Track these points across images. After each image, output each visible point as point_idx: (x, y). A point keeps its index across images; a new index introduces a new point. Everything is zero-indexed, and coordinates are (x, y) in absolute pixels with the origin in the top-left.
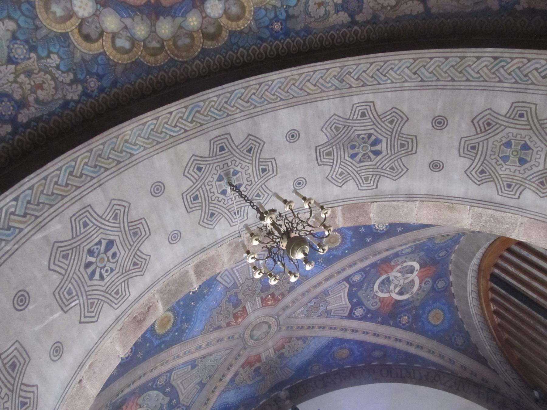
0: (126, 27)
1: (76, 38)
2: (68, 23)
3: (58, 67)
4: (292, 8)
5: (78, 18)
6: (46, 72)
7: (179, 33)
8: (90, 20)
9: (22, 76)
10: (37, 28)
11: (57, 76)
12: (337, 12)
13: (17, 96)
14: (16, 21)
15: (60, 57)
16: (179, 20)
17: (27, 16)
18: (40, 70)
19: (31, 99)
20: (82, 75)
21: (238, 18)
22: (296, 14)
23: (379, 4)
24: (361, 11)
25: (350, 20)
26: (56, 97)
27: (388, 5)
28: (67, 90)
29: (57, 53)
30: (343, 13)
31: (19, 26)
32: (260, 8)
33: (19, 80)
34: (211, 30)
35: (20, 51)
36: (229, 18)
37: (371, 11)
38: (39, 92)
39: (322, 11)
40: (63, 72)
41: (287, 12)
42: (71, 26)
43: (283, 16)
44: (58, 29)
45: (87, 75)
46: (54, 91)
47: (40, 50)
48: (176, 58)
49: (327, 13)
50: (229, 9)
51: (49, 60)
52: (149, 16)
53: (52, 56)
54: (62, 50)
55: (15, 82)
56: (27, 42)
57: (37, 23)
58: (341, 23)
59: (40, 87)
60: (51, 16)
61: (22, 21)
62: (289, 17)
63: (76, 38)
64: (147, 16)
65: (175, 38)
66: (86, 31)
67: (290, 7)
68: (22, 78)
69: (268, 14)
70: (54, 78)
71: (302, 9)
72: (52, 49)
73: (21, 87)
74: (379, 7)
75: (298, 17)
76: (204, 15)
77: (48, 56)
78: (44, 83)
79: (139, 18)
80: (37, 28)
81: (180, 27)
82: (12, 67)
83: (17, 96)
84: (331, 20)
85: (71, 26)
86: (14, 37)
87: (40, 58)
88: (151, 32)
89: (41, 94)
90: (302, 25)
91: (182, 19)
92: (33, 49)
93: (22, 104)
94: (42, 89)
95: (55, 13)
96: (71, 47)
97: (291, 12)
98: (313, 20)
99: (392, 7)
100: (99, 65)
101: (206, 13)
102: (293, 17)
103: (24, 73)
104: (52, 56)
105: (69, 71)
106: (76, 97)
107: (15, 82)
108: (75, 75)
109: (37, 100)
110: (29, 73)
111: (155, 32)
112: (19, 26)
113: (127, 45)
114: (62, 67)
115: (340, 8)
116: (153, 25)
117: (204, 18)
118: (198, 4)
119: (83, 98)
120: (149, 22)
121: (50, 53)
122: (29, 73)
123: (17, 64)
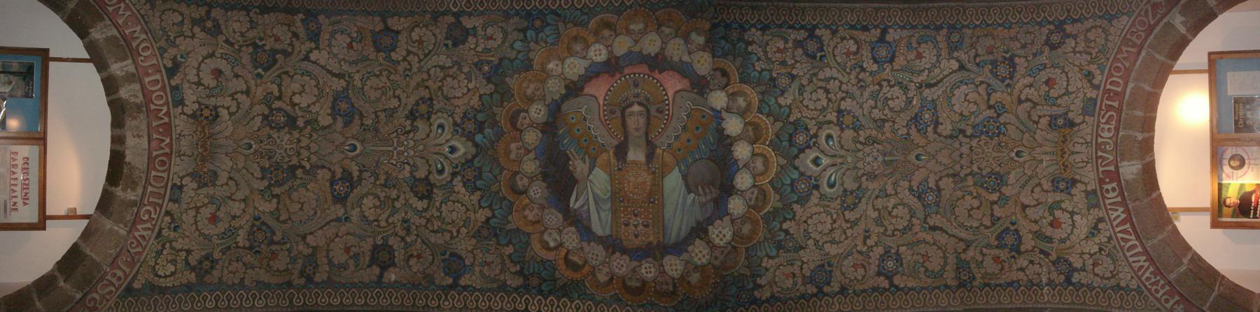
0: (690, 53)
1: (735, 76)
2: (736, 90)
3: (759, 59)
4: (520, 38)
5: (726, 91)
6: (770, 59)
7: (640, 36)
8: (717, 87)
9: (789, 63)
10: (763, 93)
11: (762, 53)
12: (474, 28)
13: (800, 51)
14: (777, 102)
15: (754, 66)
16: (637, 49)
17: (767, 103)
18: (773, 62)
19: (790, 44)
20: (740, 47)
21: (576, 39)
22: (516, 32)
23: (431, 31)
24: (449, 26)
25: (461, 19)
26: (770, 37)
27: (421, 28)
28: (758, 39)
29: (755, 70)
30: (468, 27)
31: (776, 98)
32: (552, 44)
33: (793, 62)
34: (606, 33)
35: (784, 81)
36: (585, 41)
37: (439, 24)
38: (782, 47)
39: (490, 31)
40: (756, 54)
41: (525, 36)
42: (735, 86)
43: (530, 33)
44: (747, 88)
45: (736, 45)
46: (769, 43)
47: (768, 77)
48: (648, 270)
49: (485, 28)
50: (583, 49)
51: (764, 67)
52: (665, 58)
53: (760, 70)
54: (750, 71)
55: (796, 62)
56: (775, 86)
57: (760, 97)
58: (472, 17)
59: (779, 51)
60: (748, 99)
61: (772, 102)
62: (524, 31)
63: (735, 76)
64: (666, 59)
65: (644, 32)
66: (724, 80)
67: (521, 41)
68: (790, 62)
69: (544, 37)
70: (766, 52)
71: (510, 37)
72: (756, 74)
73: (794, 56)
74: (430, 28)
75: (515, 30)
76: (610, 48)
77: (763, 70)
78: (775, 52)
79: (674, 59)
80: (763, 93)
81: (636, 42)
82: (795, 72)
83: (800, 51)
84: (481, 21)
85: (735, 86)
86: (783, 93)
87: (770, 71)
88: (666, 43)
89: (781, 45)
90: (511, 21)
91: (633, 49)
92: (773, 79)
93: (798, 44)
94: (778, 48)
95: (745, 100)
96: (741, 70)
97: (521, 36)
98: (500, 24)
99: (417, 26)
100: (723, 49)
101: (608, 50)
102: (519, 31)
103: (787, 65)
104: (760, 70)
105: (750, 53)
106: (753, 30)
107: (796, 62)
108: (746, 49)
109: (786, 41)
110: (783, 63)
111: (662, 43)
112: (776, 98)
113: (694, 36)
114: (756, 58)
115: (471, 32)
116: (663, 49)
117: (611, 46)
118: (613, 60)
119: (747, 27)
120: (666, 53)
121: (760, 73)
122: (783, 63)
123: (790, 74)
